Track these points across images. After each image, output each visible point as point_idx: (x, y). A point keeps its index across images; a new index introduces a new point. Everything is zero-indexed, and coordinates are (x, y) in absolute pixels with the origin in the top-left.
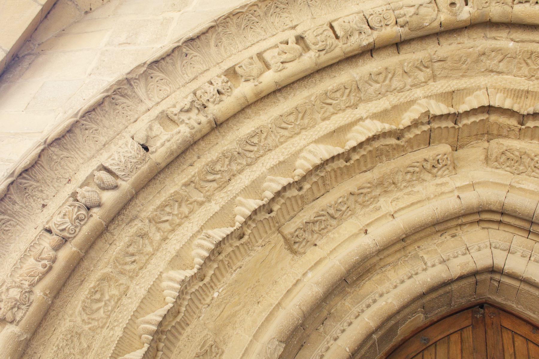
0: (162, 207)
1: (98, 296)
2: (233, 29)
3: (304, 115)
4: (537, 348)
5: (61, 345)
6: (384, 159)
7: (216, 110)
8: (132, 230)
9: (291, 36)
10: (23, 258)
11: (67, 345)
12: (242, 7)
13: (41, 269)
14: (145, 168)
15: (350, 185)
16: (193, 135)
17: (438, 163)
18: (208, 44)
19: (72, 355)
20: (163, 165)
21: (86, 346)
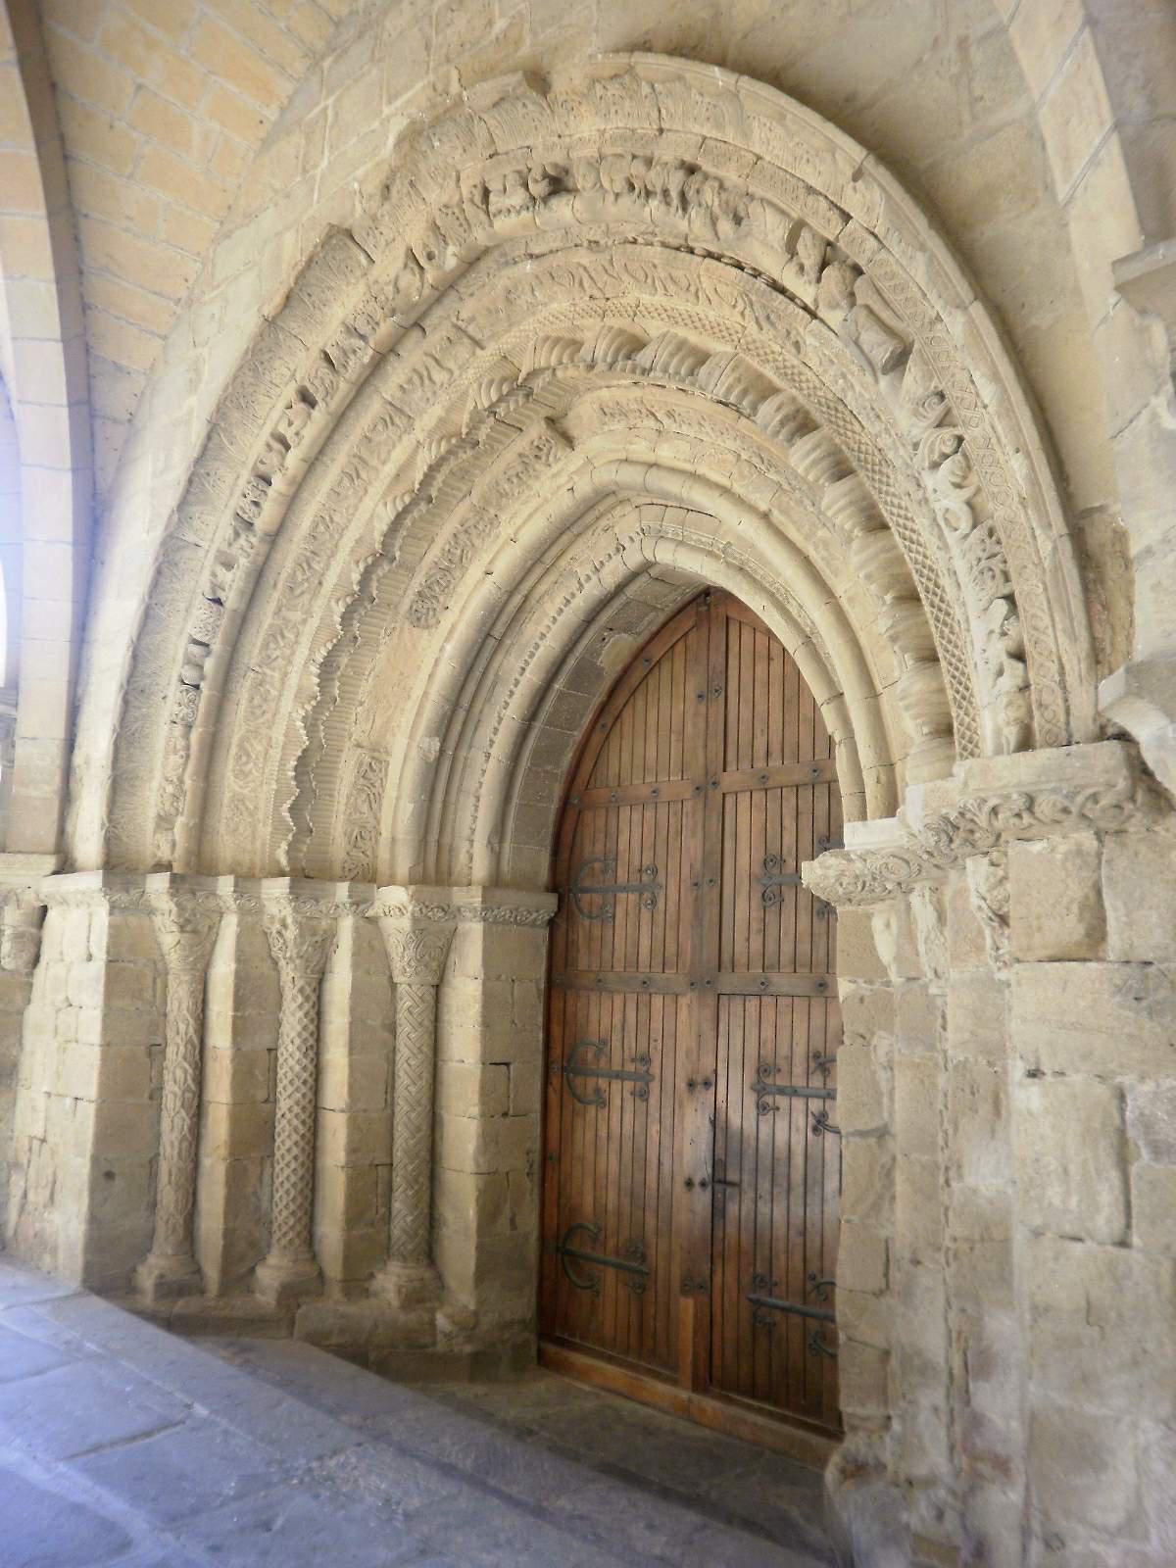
0: (265, 646)
1: (244, 759)
2: (236, 415)
6: (131, 765)
7: (264, 520)
8: (248, 684)
9: (290, 393)
10: (166, 758)
12: (225, 390)
13: (181, 761)
14: (224, 622)
15: (449, 526)
16: (253, 563)
17: (540, 449)
18: (222, 448)
20: (243, 606)
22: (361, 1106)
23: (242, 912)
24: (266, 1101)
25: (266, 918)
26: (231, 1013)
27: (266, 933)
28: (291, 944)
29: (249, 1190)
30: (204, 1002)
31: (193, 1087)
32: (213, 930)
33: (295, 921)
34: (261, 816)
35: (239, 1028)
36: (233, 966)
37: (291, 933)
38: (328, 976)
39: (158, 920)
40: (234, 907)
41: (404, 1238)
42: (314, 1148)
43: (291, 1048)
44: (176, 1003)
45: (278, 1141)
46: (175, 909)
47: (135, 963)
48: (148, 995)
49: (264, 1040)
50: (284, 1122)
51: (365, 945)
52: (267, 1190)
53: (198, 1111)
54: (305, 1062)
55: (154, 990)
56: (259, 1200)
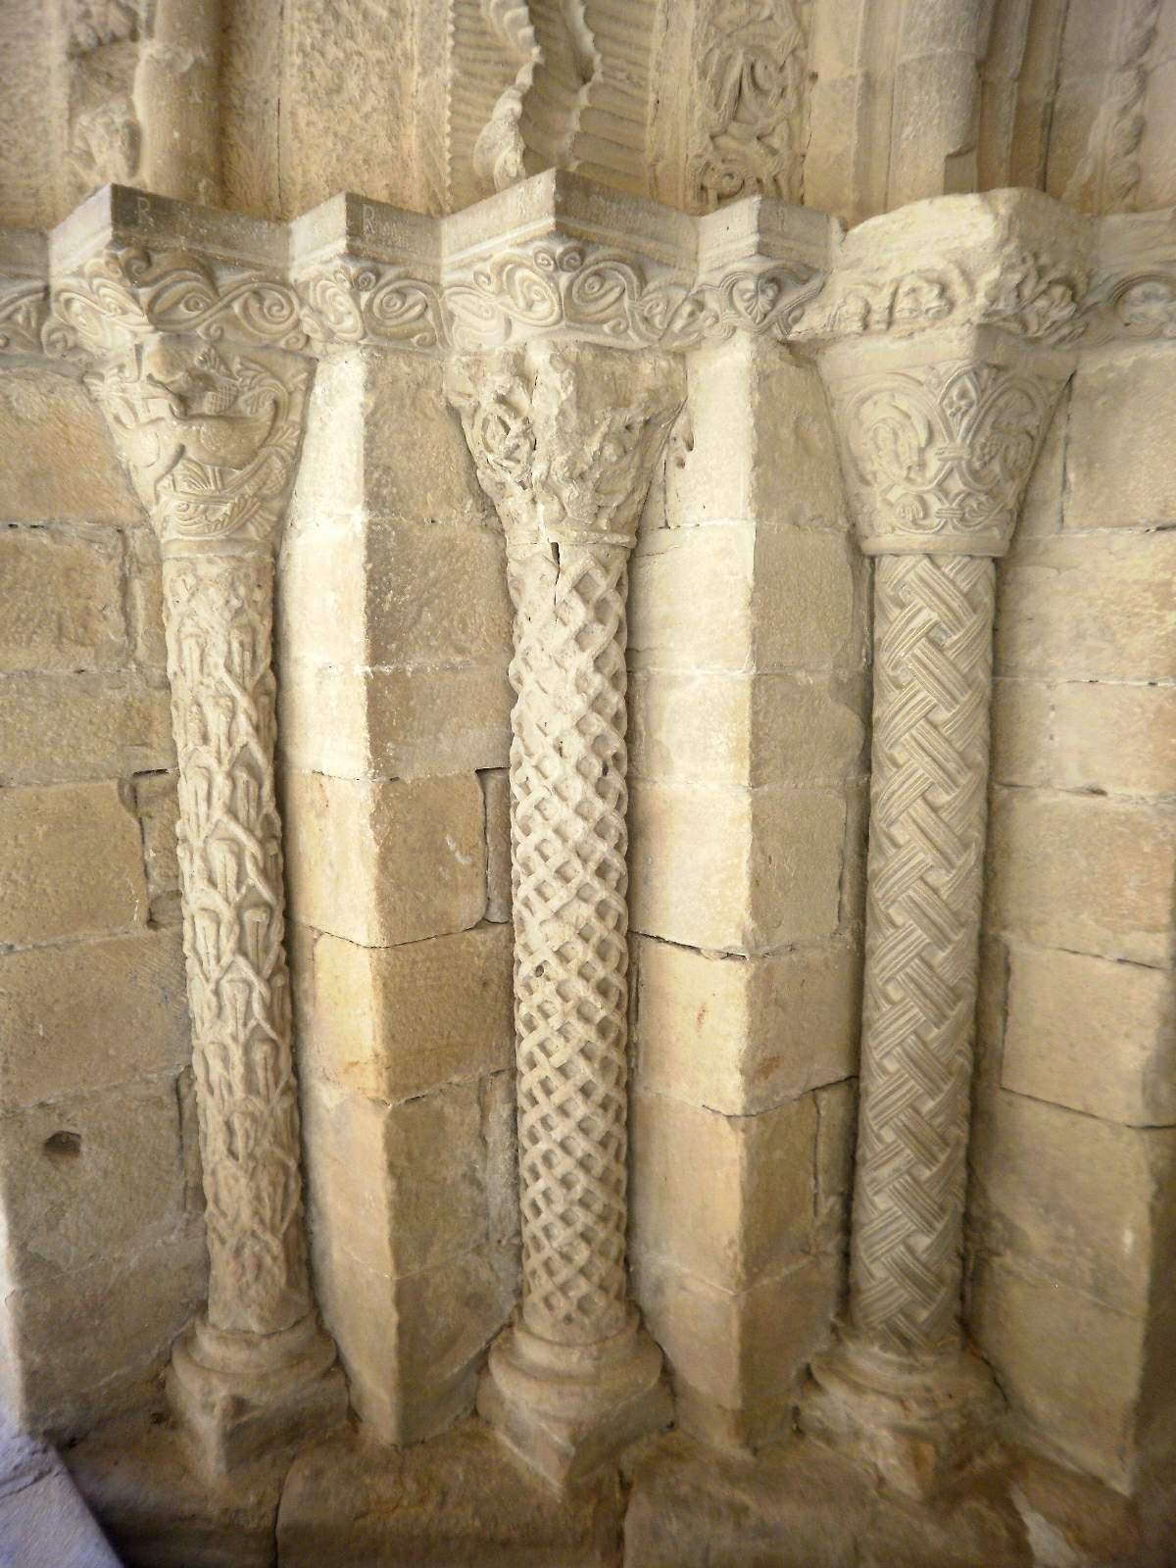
3: (949, 776)
4: (1174, 534)
5: (308, 41)
11: (325, 33)
19: (356, 58)
21: (385, 14)
22: (783, 936)
23: (383, 339)
24: (485, 923)
25: (454, 364)
26: (361, 668)
27: (454, 413)
28: (546, 435)
29: (453, 1172)
30: (277, 640)
31: (266, 894)
32: (287, 414)
33: (559, 357)
34: (412, 40)
35: (388, 716)
36: (360, 517)
37: (549, 397)
38: (661, 539)
39: (107, 388)
40: (351, 323)
41: (904, 1294)
42: (630, 1049)
43: (554, 767)
44: (191, 649)
45: (528, 1045)
46: (152, 341)
47: (57, 535)
48: (109, 629)
49: (472, 746)
50: (544, 991)
51: (785, 432)
52: (501, 1160)
53: (286, 956)
54: (600, 807)
55: (126, 612)
56: (481, 1187)
